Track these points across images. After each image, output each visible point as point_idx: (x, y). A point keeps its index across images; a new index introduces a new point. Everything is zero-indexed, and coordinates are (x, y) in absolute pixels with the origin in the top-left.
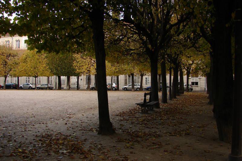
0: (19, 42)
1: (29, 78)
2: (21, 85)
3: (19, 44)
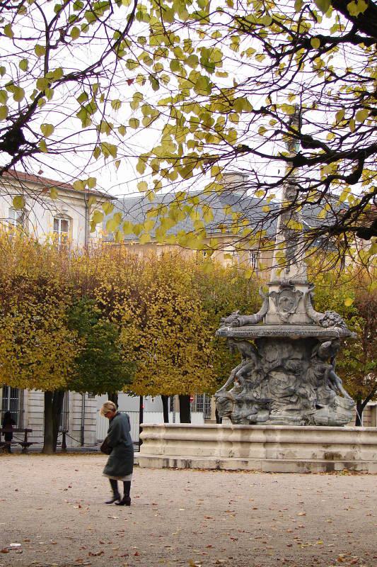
2: (140, 465)
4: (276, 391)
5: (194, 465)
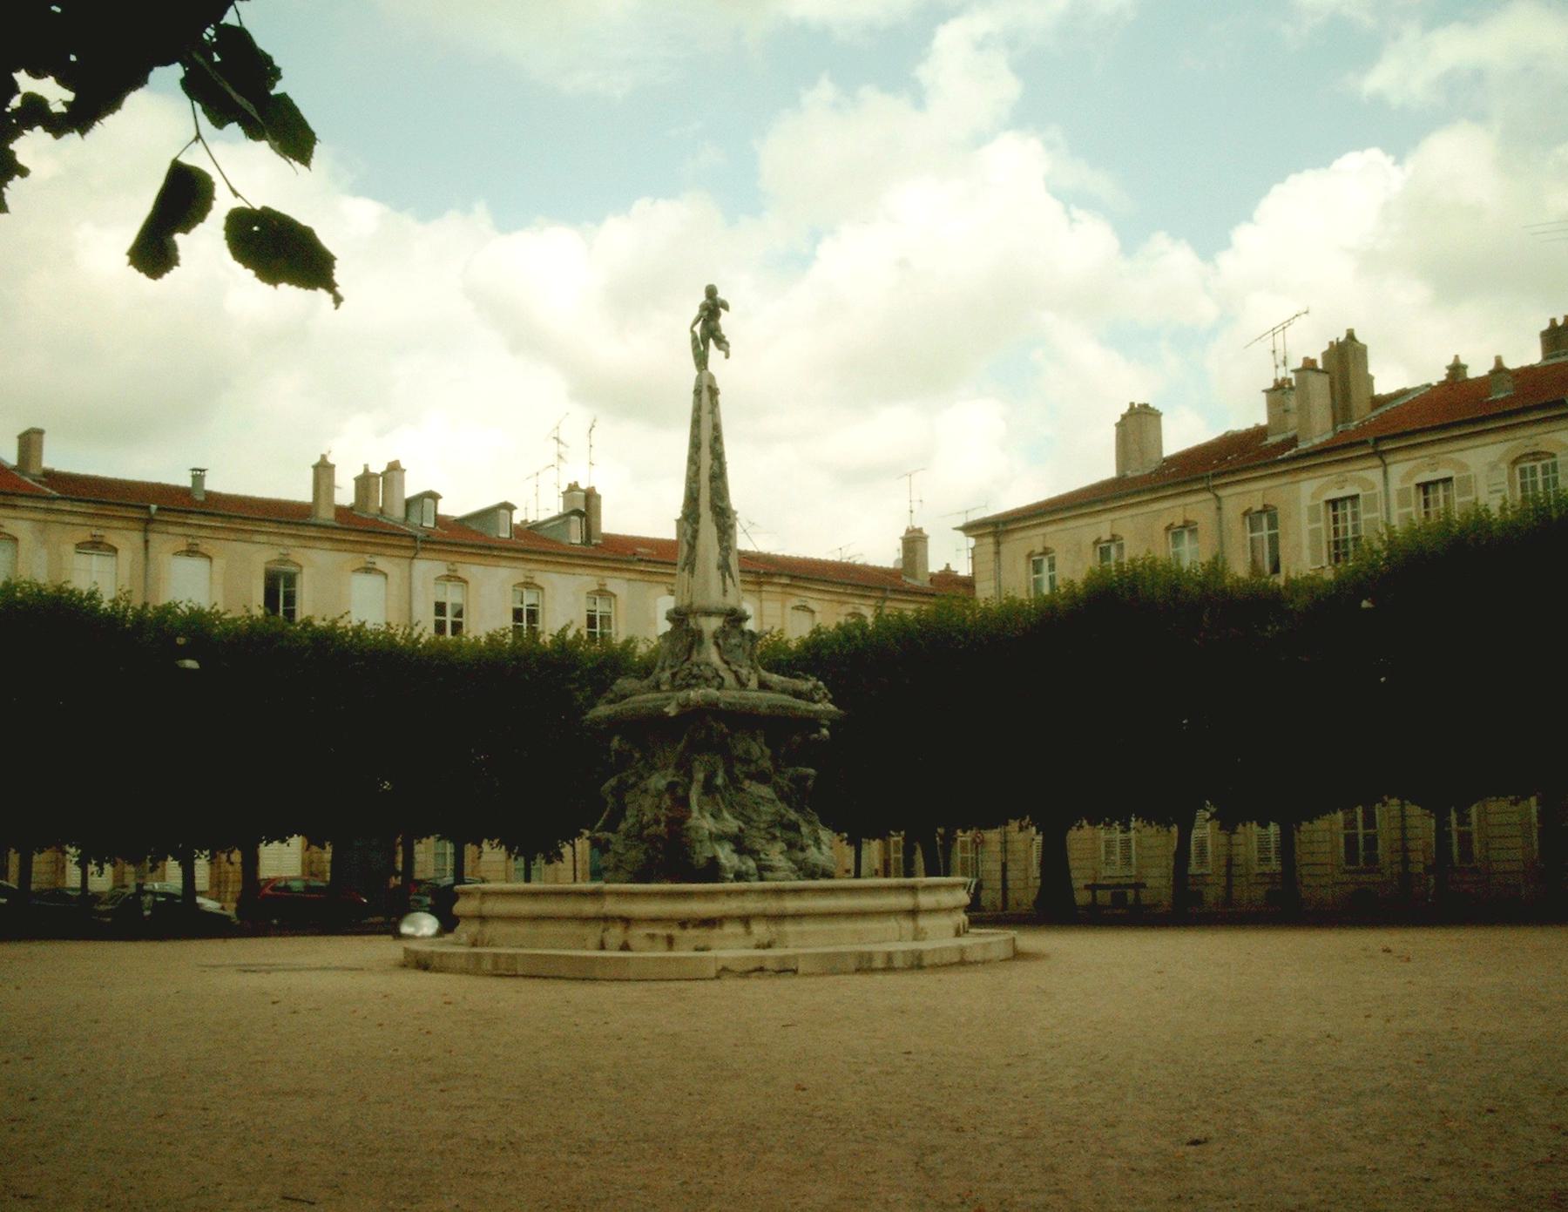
0: (1273, 524)
1: (1370, 821)
3: (1274, 540)
4: (755, 817)
5: (927, 961)
